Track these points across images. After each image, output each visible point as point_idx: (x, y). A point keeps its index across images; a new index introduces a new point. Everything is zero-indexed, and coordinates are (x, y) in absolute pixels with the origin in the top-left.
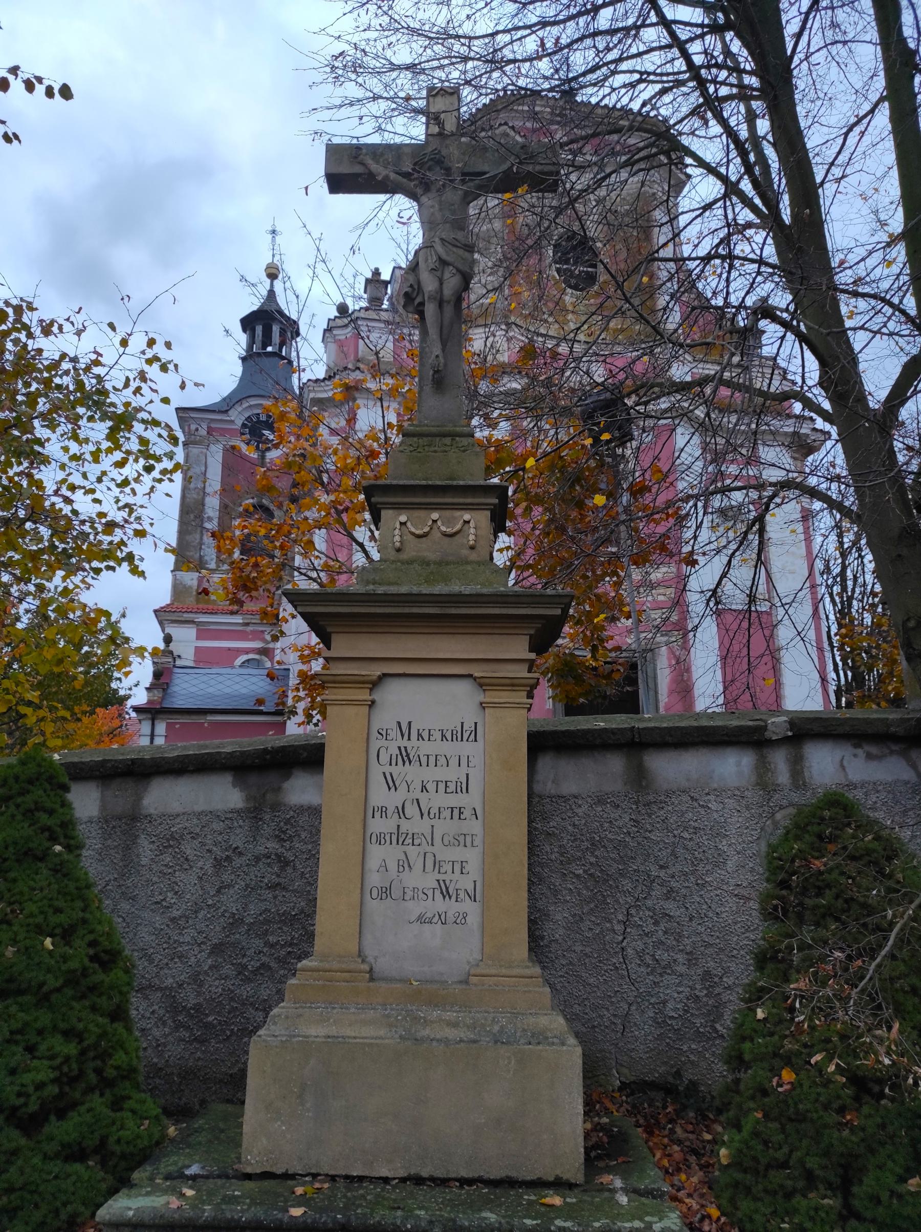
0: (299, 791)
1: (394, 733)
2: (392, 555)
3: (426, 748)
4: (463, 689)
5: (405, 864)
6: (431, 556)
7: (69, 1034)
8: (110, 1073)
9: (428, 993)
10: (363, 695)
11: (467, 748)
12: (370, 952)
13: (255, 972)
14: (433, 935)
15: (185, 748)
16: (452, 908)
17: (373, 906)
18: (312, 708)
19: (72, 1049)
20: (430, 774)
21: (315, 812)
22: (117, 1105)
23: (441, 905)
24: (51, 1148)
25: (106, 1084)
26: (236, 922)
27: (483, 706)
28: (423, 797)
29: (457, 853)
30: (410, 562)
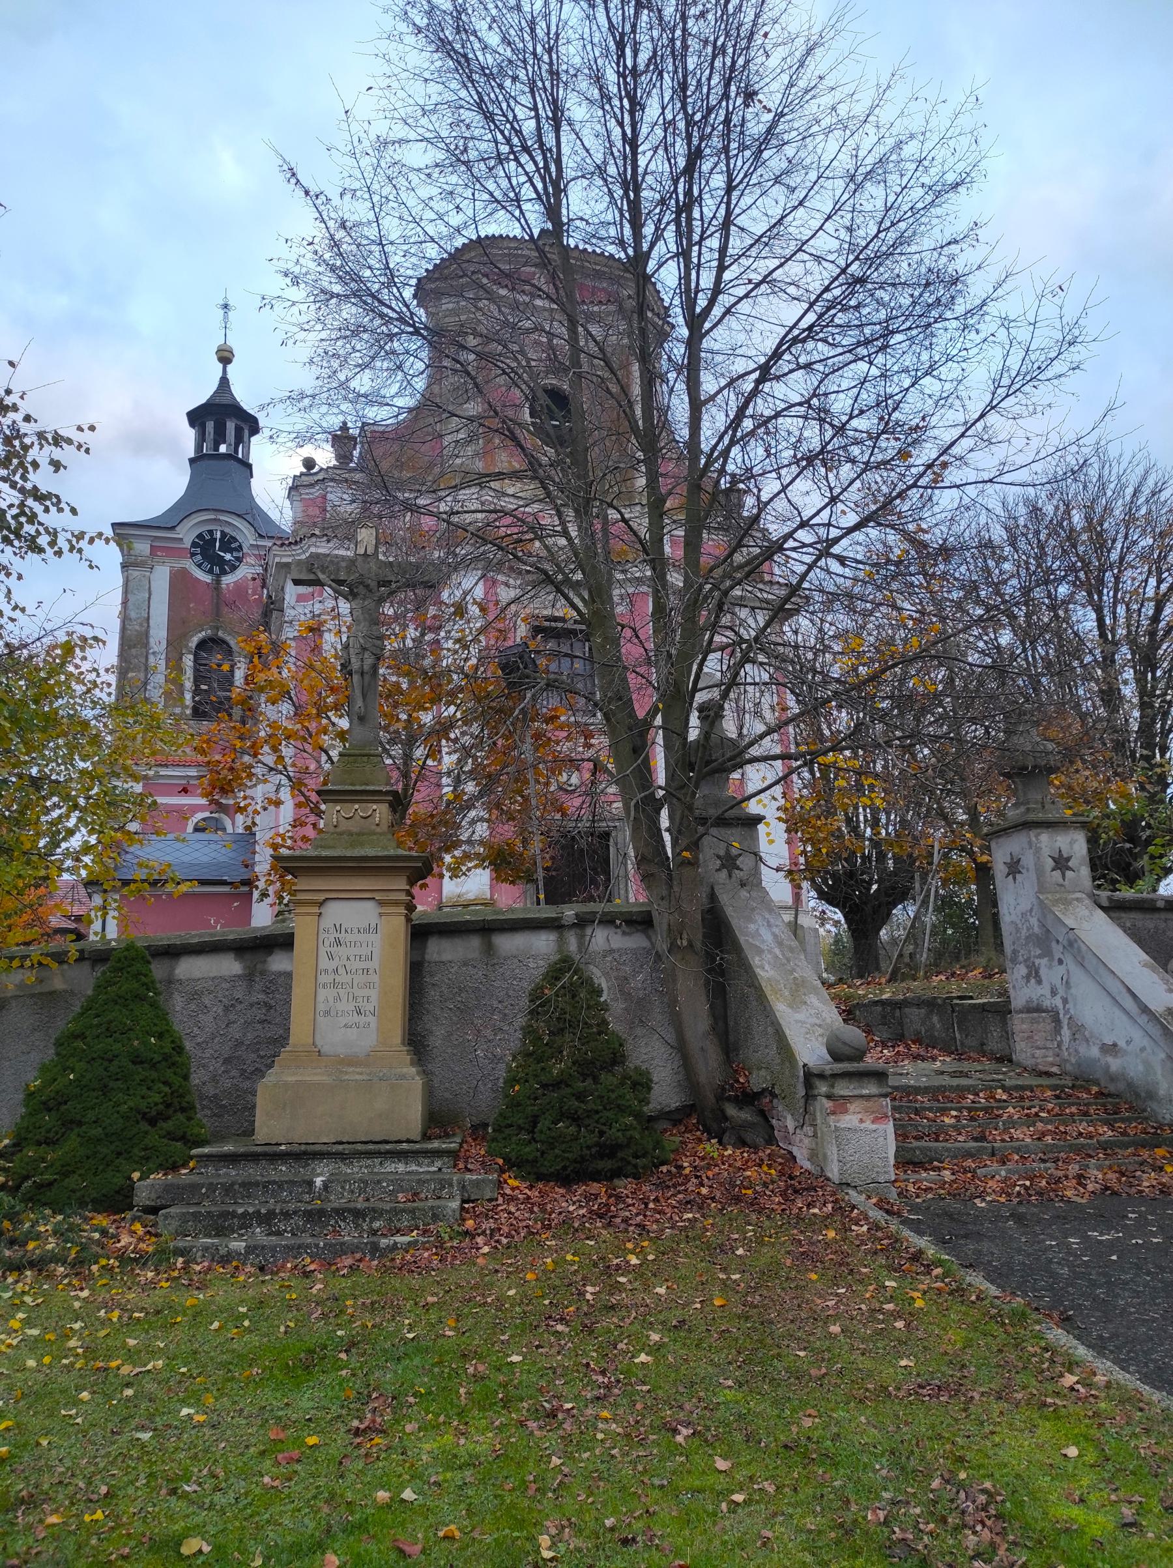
0: (278, 963)
1: (332, 930)
2: (332, 829)
3: (350, 937)
4: (370, 905)
5: (338, 998)
6: (355, 830)
7: (165, 1083)
8: (184, 1105)
9: (351, 1061)
10: (316, 910)
11: (372, 937)
12: (319, 1043)
13: (252, 1073)
14: (352, 1034)
15: (200, 936)
16: (362, 1020)
17: (321, 1019)
18: (283, 890)
19: (167, 1089)
20: (352, 951)
21: (289, 975)
22: (189, 1119)
23: (356, 1018)
24: (163, 1133)
25: (183, 1110)
26: (239, 1044)
27: (381, 915)
28: (348, 964)
29: (366, 992)
30: (341, 834)
